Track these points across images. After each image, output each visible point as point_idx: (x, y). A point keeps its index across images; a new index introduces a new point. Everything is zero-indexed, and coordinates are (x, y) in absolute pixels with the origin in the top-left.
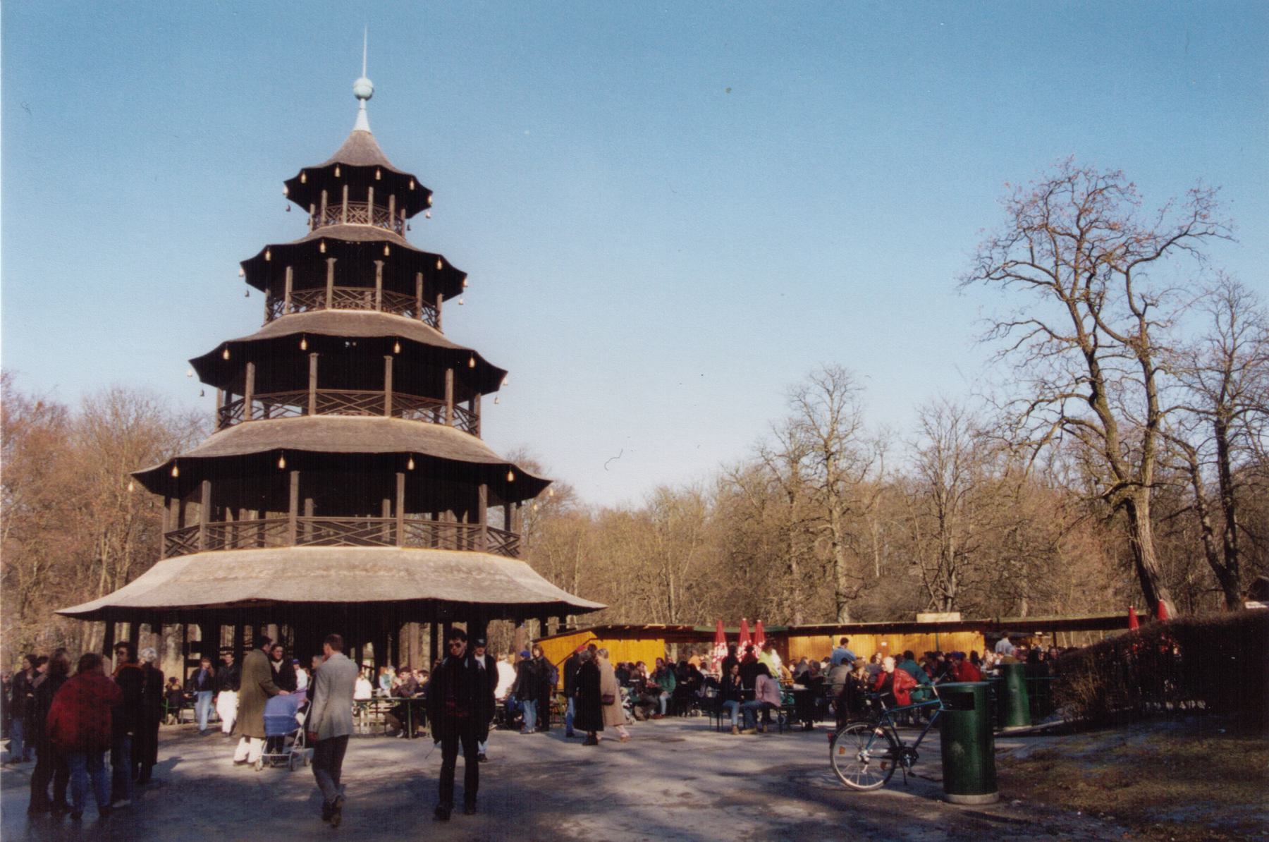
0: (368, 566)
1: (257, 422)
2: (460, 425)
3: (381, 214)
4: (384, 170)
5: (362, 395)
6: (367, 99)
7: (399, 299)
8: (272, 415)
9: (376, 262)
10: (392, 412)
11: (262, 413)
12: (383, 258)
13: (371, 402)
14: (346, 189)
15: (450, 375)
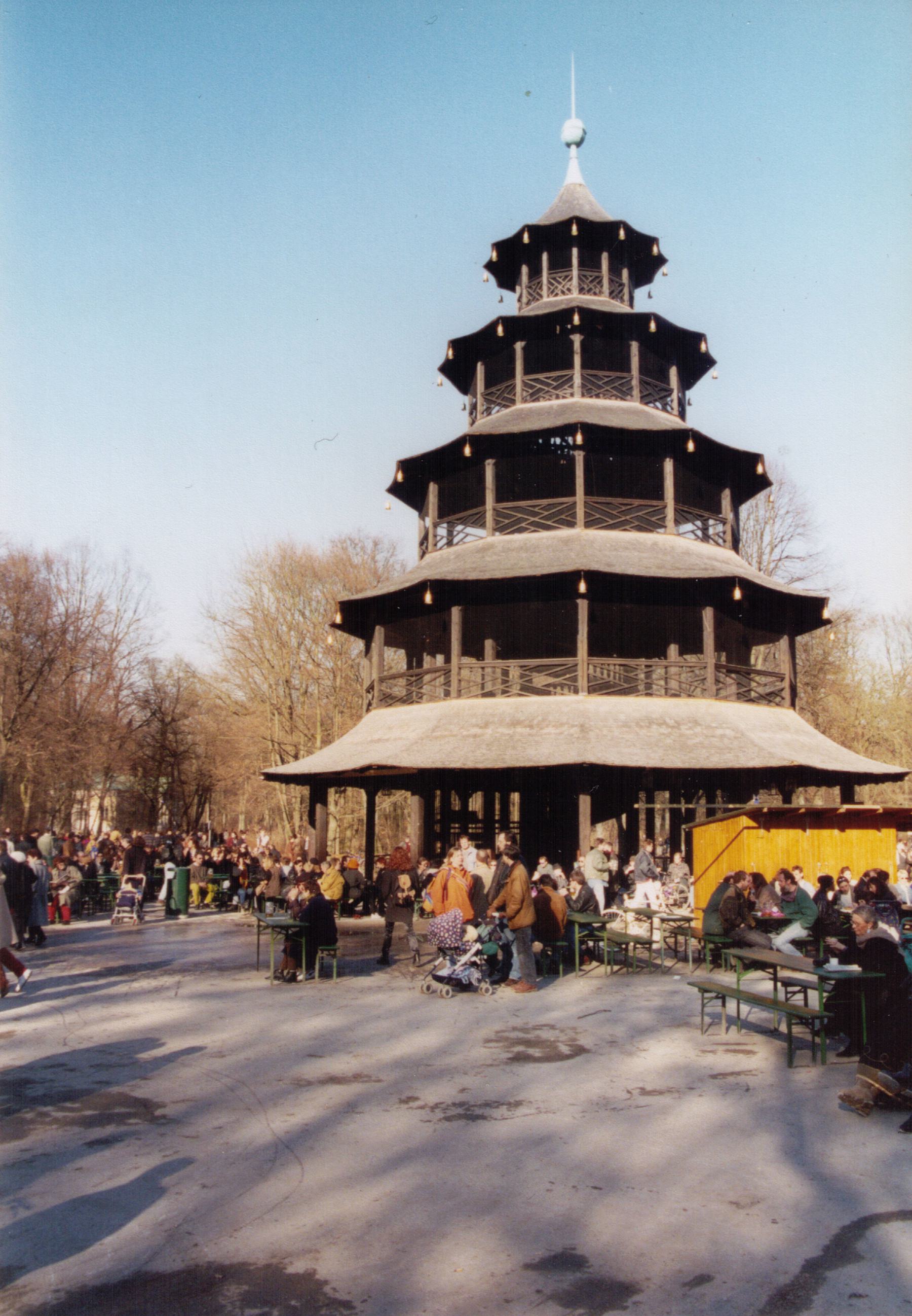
0: (535, 722)
1: (441, 552)
2: (693, 532)
3: (591, 279)
4: (582, 222)
5: (549, 505)
6: (579, 144)
7: (606, 380)
8: (456, 540)
9: (572, 337)
10: (585, 523)
11: (444, 541)
12: (575, 329)
13: (561, 512)
14: (545, 257)
15: (669, 466)
